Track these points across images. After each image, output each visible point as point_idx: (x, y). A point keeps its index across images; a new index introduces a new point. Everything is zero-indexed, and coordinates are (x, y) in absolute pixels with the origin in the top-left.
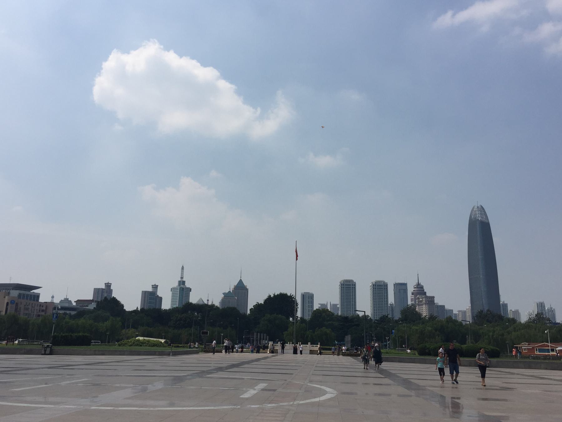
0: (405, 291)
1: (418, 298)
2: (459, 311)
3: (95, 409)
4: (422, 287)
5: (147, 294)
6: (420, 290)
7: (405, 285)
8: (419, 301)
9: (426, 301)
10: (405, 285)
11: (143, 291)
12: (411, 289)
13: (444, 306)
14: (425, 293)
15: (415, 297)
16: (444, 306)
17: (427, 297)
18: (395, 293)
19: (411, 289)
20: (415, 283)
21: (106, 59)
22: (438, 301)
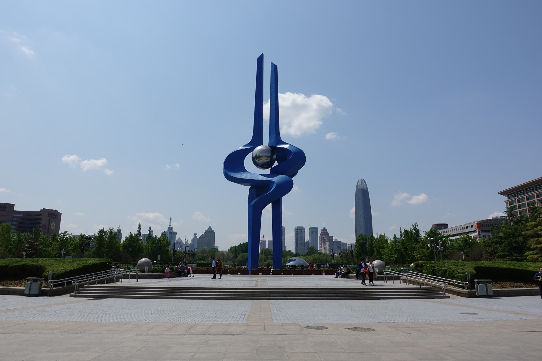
0: (317, 233)
4: (326, 230)
7: (316, 228)
10: (316, 228)
12: (319, 232)
14: (328, 234)
19: (319, 232)
20: (322, 228)
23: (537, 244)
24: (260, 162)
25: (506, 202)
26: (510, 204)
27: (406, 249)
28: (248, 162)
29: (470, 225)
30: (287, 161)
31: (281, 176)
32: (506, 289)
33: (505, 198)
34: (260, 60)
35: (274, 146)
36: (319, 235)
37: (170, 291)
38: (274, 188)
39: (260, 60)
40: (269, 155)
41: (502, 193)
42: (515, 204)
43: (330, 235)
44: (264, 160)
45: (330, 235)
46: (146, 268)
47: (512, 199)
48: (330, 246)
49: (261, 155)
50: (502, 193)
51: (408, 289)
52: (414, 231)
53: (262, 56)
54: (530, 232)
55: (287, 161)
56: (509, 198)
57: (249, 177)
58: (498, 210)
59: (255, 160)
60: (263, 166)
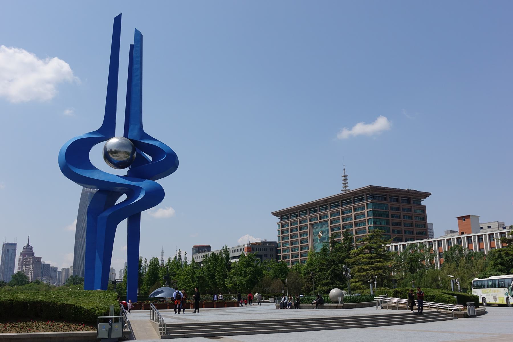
0: (14, 251)
1: (26, 259)
2: (63, 269)
3: (101, 318)
4: (31, 248)
5: (13, 247)
6: (28, 250)
7: (14, 245)
8: (26, 262)
9: (33, 261)
10: (14, 245)
11: (3, 244)
12: (19, 250)
13: (50, 265)
14: (33, 254)
15: (23, 257)
16: (50, 265)
17: (35, 258)
18: (2, 253)
19: (19, 250)
20: (25, 244)
21: (8, 46)
22: (45, 260)
23: (359, 271)
24: (115, 158)
25: (278, 224)
26: (283, 227)
27: (212, 277)
28: (96, 155)
29: (240, 248)
30: (150, 162)
31: (147, 181)
32: (29, 333)
33: (278, 220)
34: (118, 21)
35: (137, 139)
36: (18, 256)
37: (356, 321)
38: (141, 196)
39: (118, 21)
40: (129, 151)
41: (276, 214)
42: (287, 228)
43: (36, 255)
44: (122, 157)
45: (36, 255)
46: (340, 299)
47: (285, 221)
48: (35, 271)
49: (118, 149)
50: (276, 214)
51: (392, 315)
52: (224, 255)
53: (121, 14)
54: (353, 260)
55: (150, 162)
56: (282, 220)
57: (95, 176)
58: (270, 232)
59: (108, 156)
60: (119, 165)
